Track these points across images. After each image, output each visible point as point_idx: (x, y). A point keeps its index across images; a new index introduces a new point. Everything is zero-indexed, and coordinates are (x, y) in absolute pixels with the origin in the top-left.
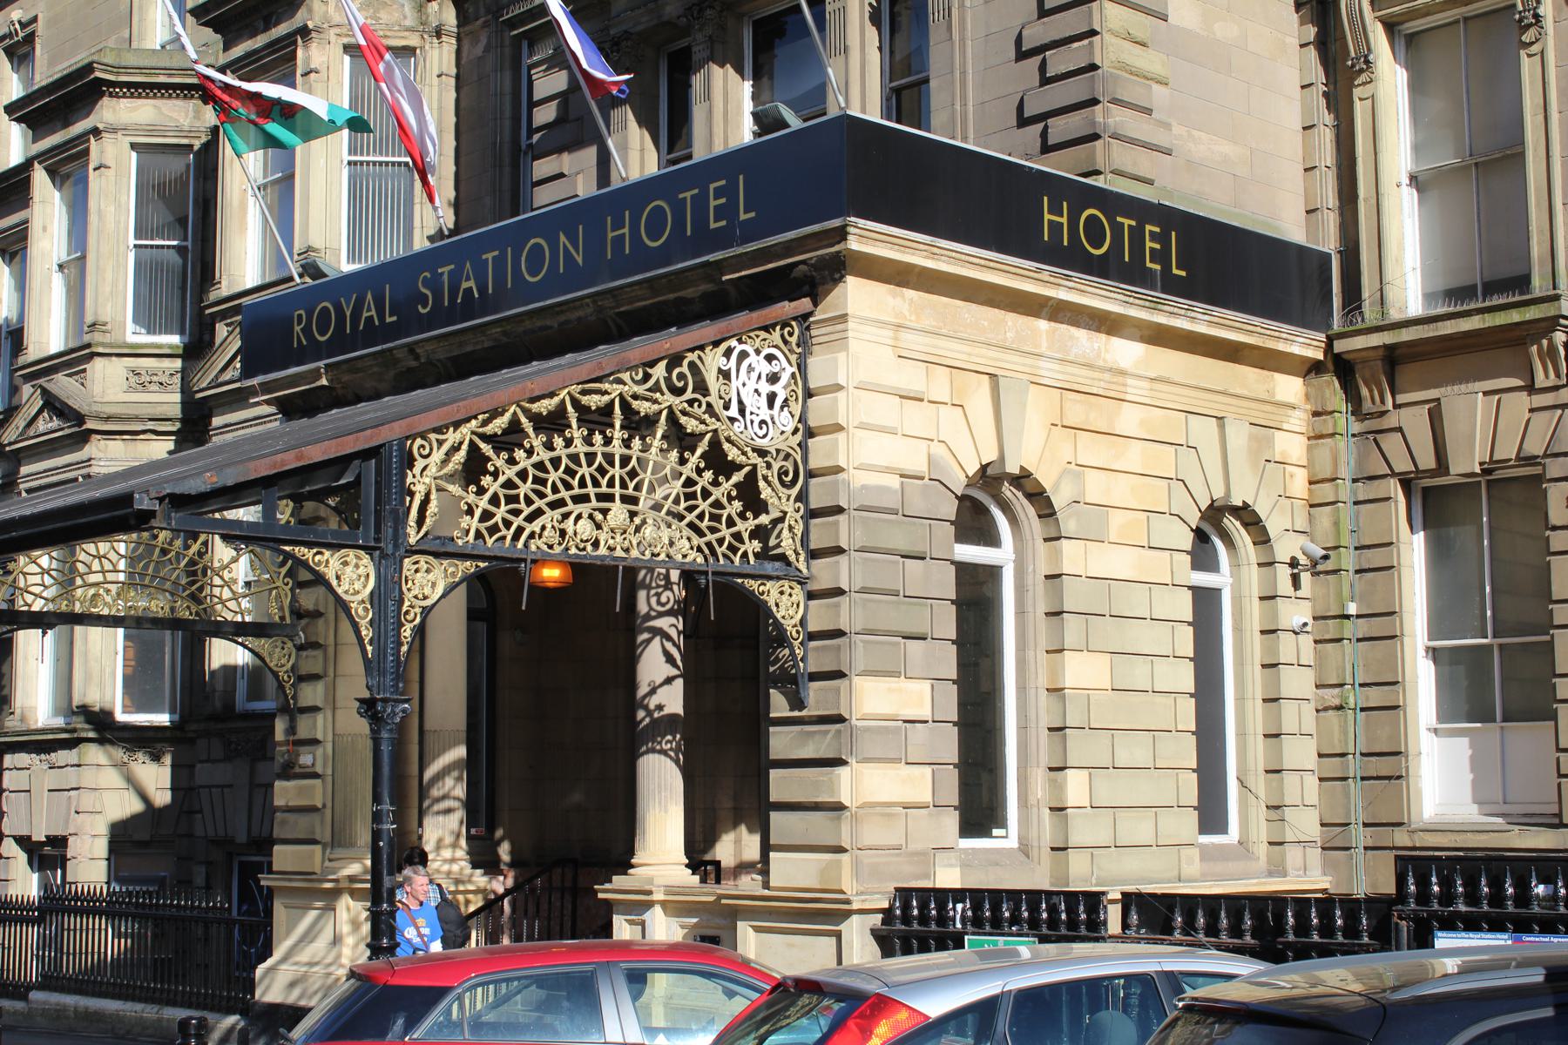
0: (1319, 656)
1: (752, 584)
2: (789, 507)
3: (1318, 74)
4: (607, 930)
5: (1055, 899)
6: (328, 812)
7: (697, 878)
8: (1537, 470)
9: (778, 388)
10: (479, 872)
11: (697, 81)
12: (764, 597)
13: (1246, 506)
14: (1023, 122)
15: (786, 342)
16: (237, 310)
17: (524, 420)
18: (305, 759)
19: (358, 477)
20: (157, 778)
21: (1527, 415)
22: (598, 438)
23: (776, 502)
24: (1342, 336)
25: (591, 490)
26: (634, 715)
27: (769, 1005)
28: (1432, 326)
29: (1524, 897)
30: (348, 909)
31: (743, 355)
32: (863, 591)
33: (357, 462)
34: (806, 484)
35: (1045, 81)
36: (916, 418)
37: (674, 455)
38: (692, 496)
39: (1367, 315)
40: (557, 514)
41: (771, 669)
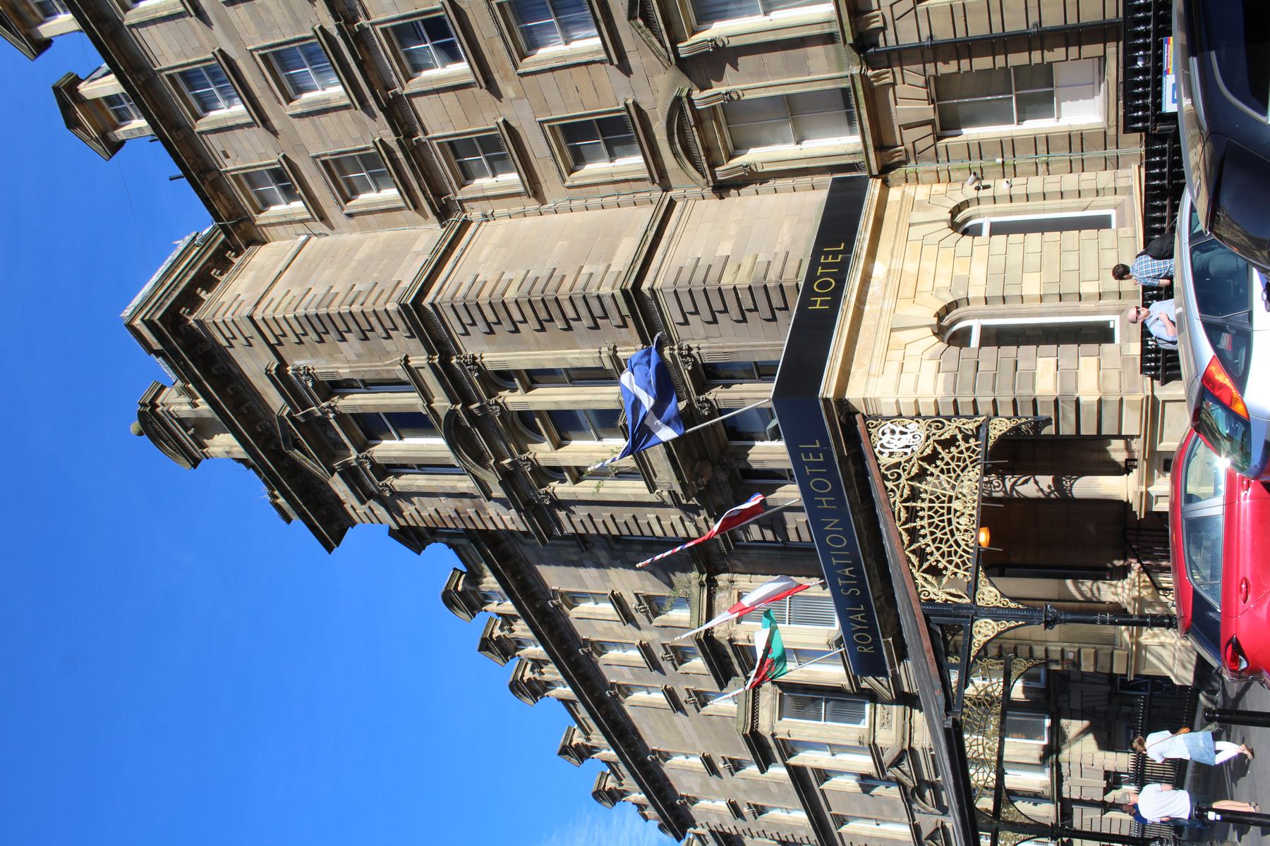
0: (1023, 174)
1: (991, 442)
2: (954, 425)
3: (752, 188)
4: (1162, 515)
5: (1147, 297)
6: (1097, 646)
7: (1134, 470)
8: (932, 79)
9: (897, 430)
10: (1129, 575)
11: (755, 466)
12: (997, 437)
13: (951, 212)
14: (774, 319)
15: (876, 426)
16: (855, 678)
17: (912, 548)
18: (1071, 656)
19: (938, 625)
20: (1073, 727)
21: (906, 85)
22: (921, 514)
23: (951, 431)
24: (870, 171)
25: (945, 517)
26: (1053, 499)
27: (1205, 434)
28: (865, 130)
29: (1144, 71)
30: (1146, 639)
31: (882, 446)
32: (994, 390)
33: (931, 625)
34: (943, 417)
35: (756, 309)
36: (911, 366)
37: (929, 478)
38: (949, 471)
39: (860, 160)
40: (957, 533)
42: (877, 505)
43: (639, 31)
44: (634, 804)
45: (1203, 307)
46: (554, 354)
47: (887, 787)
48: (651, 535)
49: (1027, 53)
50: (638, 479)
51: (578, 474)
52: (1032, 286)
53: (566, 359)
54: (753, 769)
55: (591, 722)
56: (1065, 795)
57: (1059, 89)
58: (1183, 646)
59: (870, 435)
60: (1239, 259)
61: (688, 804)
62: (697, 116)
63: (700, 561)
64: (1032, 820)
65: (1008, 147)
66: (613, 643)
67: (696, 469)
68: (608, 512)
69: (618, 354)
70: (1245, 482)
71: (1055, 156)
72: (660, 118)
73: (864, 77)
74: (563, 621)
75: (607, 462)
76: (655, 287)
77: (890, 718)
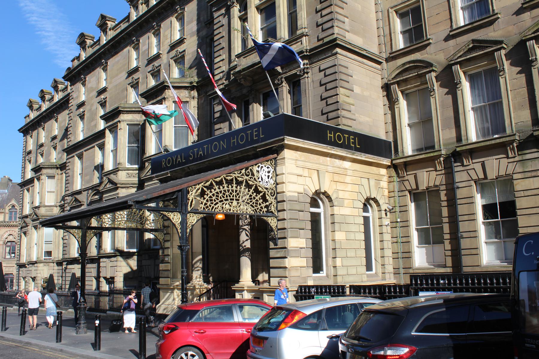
0: (392, 231)
1: (265, 218)
2: (273, 201)
3: (387, 103)
6: (172, 271)
7: (254, 284)
8: (438, 188)
9: (270, 174)
10: (205, 284)
11: (251, 107)
12: (268, 221)
13: (375, 198)
15: (271, 164)
18: (166, 259)
20: (133, 263)
21: (435, 176)
22: (230, 186)
23: (270, 199)
25: (229, 198)
26: (239, 248)
27: (271, 313)
28: (414, 157)
30: (176, 292)
31: (262, 167)
32: (290, 219)
33: (177, 193)
34: (277, 195)
35: (327, 105)
36: (301, 180)
37: (247, 190)
39: (400, 155)
41: (270, 237)
42: (234, 166)
43: (466, 45)
44: (80, 54)
45: (329, 310)
46: (304, 4)
47: (98, 177)
48: (215, 57)
49: (449, 232)
50: (242, 49)
51: (244, 19)
52: (339, 236)
53: (301, 10)
54: (102, 113)
55: (119, 31)
56: (101, 260)
57: (432, 247)
58: (174, 308)
59: (267, 161)
60: (350, 325)
61: (82, 82)
62: (423, 75)
63: (203, 82)
64: (88, 244)
65: (405, 224)
66: (160, 40)
67: (248, 78)
68: (225, 35)
69: (304, 37)
70: (249, 330)
71: (400, 246)
72: (422, 57)
73: (440, 156)
74: (169, 14)
75: (250, 32)
76: (338, 55)
77: (132, 177)
